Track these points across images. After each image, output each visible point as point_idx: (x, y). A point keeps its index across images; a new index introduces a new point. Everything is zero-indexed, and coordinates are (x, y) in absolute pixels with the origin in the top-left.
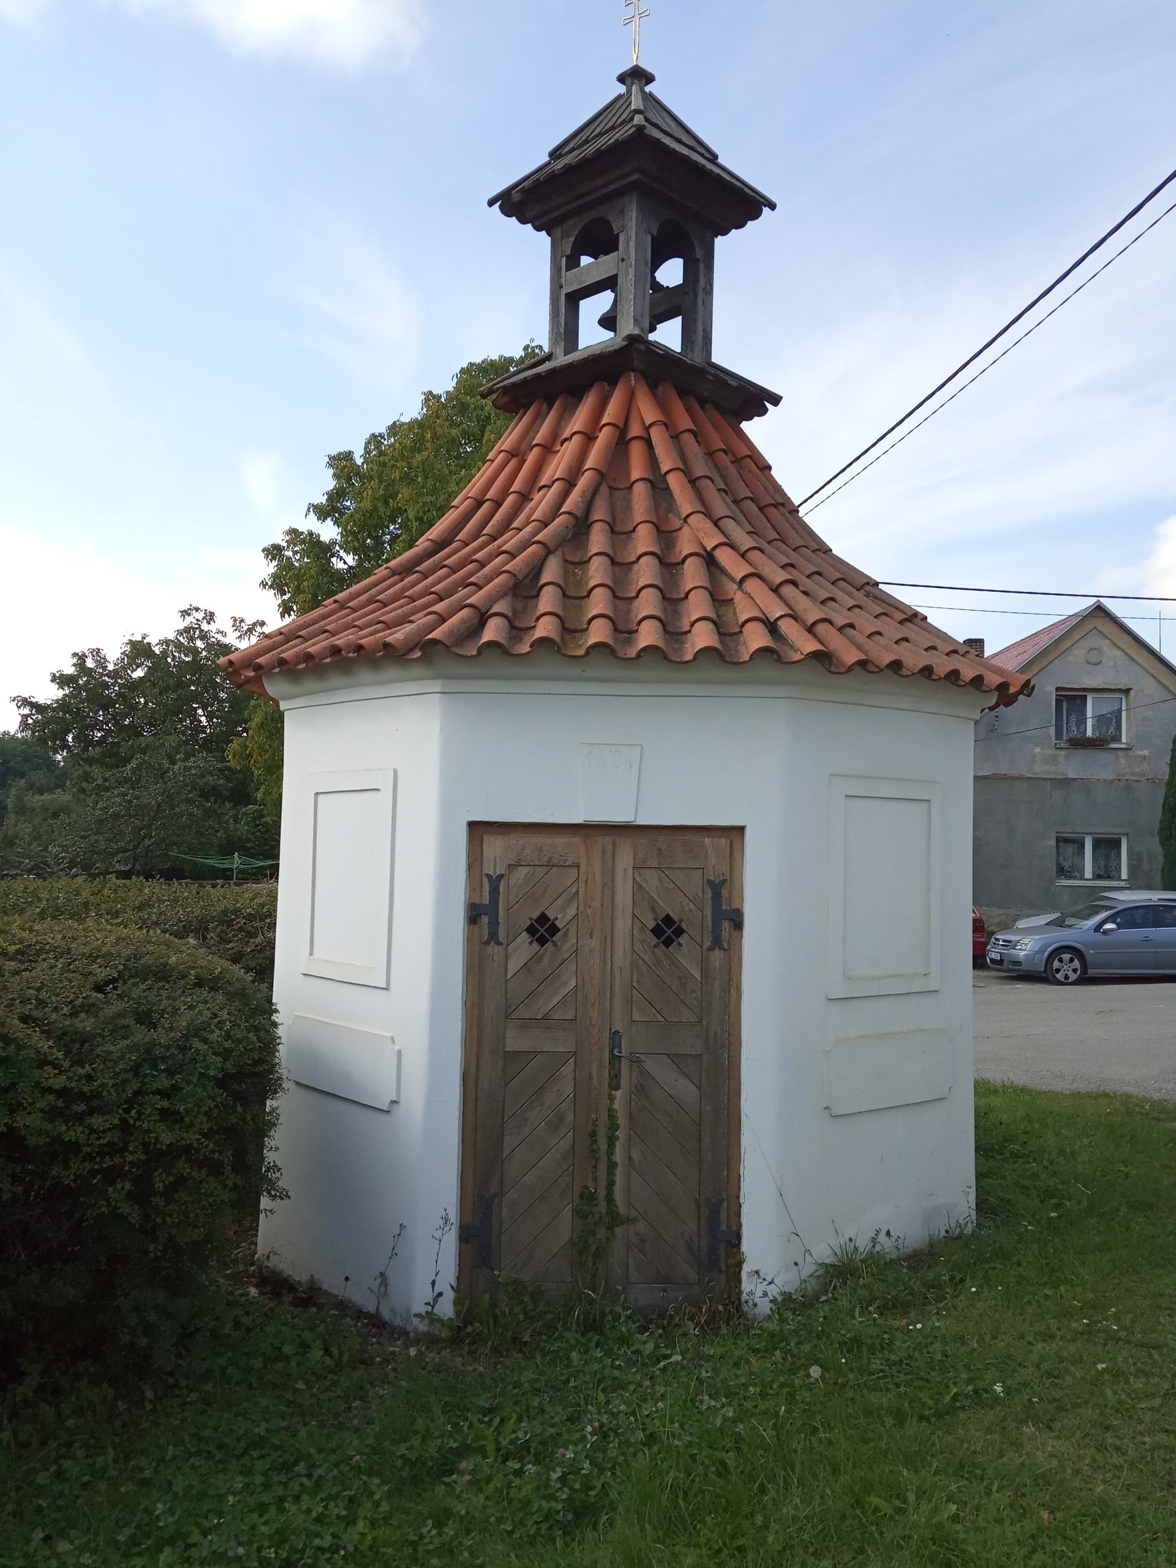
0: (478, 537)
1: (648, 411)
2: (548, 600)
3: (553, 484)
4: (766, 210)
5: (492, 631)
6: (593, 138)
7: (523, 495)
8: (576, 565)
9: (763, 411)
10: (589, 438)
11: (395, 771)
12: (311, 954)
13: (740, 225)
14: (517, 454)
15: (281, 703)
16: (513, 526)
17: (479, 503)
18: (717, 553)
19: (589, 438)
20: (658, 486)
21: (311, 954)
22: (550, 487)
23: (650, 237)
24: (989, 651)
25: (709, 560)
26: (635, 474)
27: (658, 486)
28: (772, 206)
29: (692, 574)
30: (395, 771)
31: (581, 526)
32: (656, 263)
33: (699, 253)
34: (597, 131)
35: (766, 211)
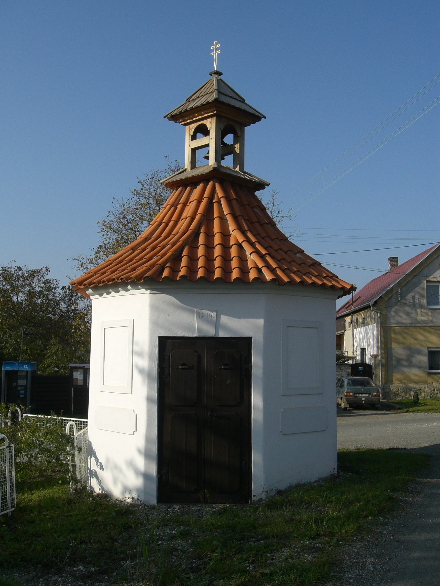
0: (161, 224)
1: (219, 193)
2: (184, 262)
3: (187, 218)
4: (263, 119)
5: (166, 273)
6: (200, 97)
7: (173, 245)
8: (194, 247)
9: (264, 188)
10: (199, 201)
11: (133, 320)
12: (104, 384)
13: (254, 123)
14: (175, 205)
15: (91, 297)
16: (172, 234)
17: (160, 223)
18: (243, 244)
19: (199, 201)
20: (222, 218)
21: (104, 384)
22: (186, 219)
23: (221, 131)
24: (400, 263)
25: (240, 246)
26: (215, 216)
27: (222, 218)
28: (265, 118)
29: (234, 252)
30: (133, 320)
31: (196, 234)
32: (223, 137)
33: (239, 134)
34: (202, 94)
35: (263, 119)
